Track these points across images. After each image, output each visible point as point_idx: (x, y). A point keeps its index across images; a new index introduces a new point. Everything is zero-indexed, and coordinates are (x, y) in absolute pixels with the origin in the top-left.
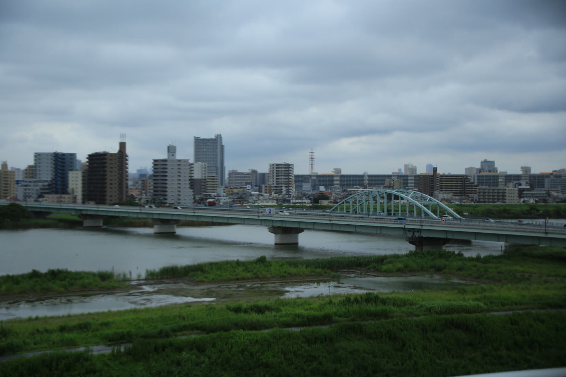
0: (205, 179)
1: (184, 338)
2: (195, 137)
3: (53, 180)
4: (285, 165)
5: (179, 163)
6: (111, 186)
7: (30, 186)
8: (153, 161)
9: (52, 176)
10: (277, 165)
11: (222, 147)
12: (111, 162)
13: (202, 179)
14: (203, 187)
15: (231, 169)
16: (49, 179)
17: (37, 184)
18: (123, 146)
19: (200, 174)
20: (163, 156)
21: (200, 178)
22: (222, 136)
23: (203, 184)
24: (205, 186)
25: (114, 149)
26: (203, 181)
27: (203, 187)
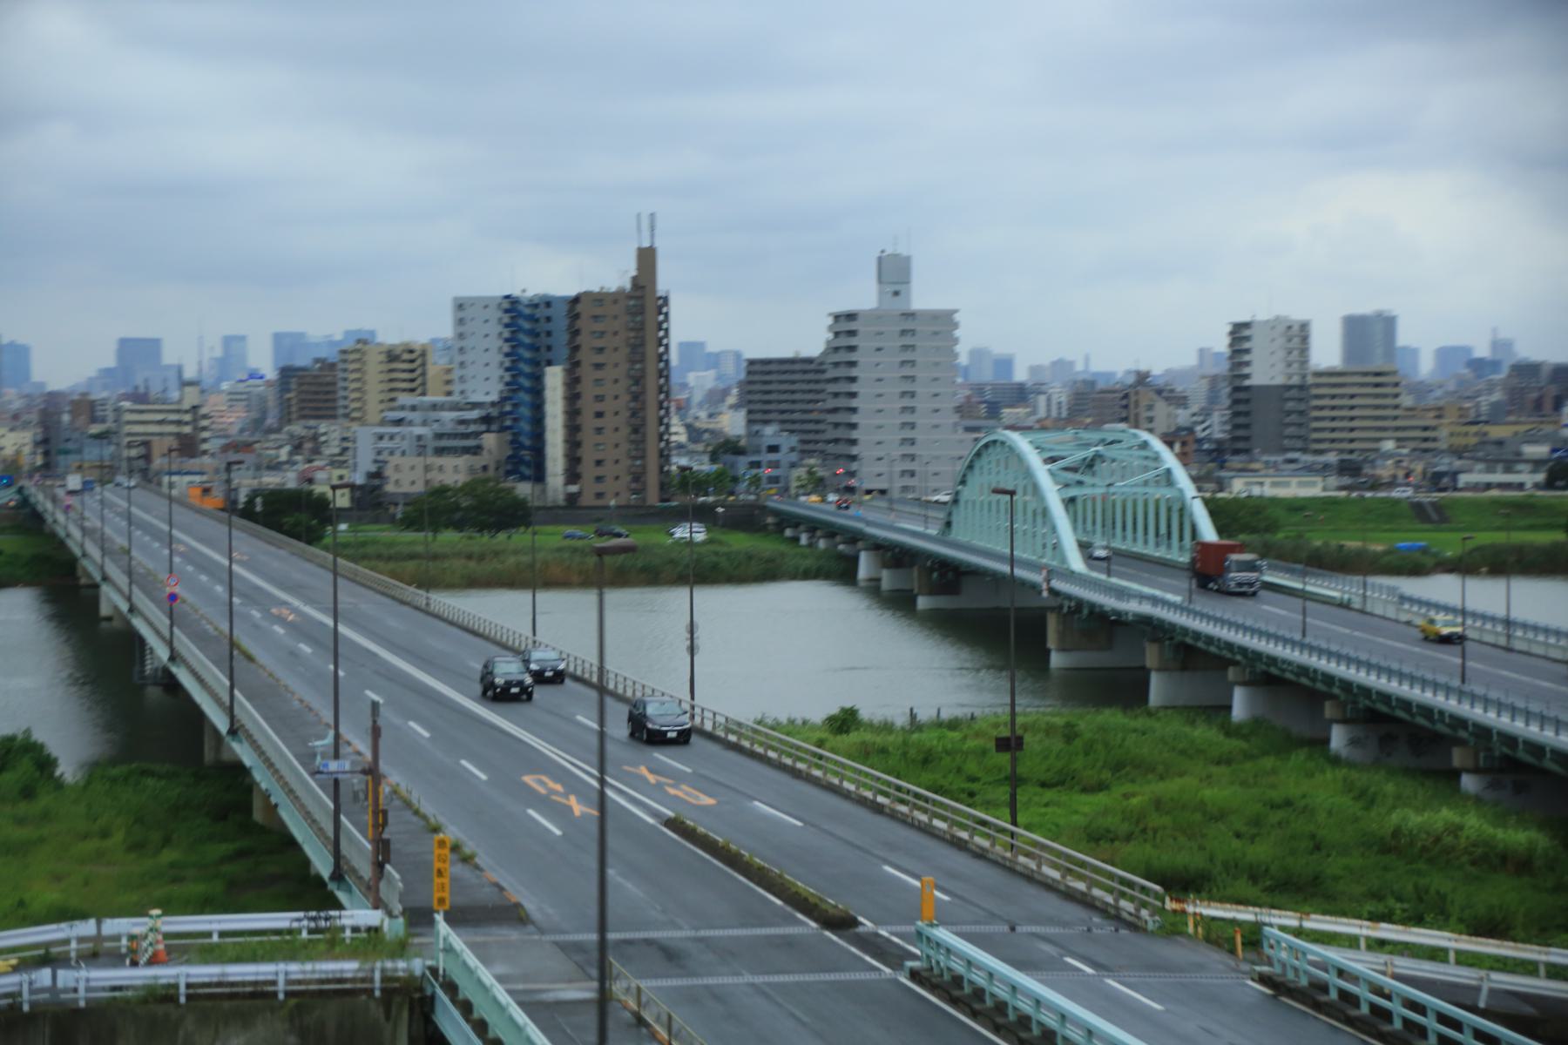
0: (1301, 387)
3: (503, 400)
5: (908, 325)
6: (599, 423)
7: (411, 423)
8: (830, 321)
9: (501, 387)
12: (599, 327)
13: (1289, 388)
14: (1294, 418)
15: (685, 339)
16: (494, 397)
18: (647, 258)
19: (1280, 366)
20: (864, 296)
21: (1279, 380)
23: (1290, 405)
24: (1301, 413)
26: (1294, 393)
27: (1294, 418)
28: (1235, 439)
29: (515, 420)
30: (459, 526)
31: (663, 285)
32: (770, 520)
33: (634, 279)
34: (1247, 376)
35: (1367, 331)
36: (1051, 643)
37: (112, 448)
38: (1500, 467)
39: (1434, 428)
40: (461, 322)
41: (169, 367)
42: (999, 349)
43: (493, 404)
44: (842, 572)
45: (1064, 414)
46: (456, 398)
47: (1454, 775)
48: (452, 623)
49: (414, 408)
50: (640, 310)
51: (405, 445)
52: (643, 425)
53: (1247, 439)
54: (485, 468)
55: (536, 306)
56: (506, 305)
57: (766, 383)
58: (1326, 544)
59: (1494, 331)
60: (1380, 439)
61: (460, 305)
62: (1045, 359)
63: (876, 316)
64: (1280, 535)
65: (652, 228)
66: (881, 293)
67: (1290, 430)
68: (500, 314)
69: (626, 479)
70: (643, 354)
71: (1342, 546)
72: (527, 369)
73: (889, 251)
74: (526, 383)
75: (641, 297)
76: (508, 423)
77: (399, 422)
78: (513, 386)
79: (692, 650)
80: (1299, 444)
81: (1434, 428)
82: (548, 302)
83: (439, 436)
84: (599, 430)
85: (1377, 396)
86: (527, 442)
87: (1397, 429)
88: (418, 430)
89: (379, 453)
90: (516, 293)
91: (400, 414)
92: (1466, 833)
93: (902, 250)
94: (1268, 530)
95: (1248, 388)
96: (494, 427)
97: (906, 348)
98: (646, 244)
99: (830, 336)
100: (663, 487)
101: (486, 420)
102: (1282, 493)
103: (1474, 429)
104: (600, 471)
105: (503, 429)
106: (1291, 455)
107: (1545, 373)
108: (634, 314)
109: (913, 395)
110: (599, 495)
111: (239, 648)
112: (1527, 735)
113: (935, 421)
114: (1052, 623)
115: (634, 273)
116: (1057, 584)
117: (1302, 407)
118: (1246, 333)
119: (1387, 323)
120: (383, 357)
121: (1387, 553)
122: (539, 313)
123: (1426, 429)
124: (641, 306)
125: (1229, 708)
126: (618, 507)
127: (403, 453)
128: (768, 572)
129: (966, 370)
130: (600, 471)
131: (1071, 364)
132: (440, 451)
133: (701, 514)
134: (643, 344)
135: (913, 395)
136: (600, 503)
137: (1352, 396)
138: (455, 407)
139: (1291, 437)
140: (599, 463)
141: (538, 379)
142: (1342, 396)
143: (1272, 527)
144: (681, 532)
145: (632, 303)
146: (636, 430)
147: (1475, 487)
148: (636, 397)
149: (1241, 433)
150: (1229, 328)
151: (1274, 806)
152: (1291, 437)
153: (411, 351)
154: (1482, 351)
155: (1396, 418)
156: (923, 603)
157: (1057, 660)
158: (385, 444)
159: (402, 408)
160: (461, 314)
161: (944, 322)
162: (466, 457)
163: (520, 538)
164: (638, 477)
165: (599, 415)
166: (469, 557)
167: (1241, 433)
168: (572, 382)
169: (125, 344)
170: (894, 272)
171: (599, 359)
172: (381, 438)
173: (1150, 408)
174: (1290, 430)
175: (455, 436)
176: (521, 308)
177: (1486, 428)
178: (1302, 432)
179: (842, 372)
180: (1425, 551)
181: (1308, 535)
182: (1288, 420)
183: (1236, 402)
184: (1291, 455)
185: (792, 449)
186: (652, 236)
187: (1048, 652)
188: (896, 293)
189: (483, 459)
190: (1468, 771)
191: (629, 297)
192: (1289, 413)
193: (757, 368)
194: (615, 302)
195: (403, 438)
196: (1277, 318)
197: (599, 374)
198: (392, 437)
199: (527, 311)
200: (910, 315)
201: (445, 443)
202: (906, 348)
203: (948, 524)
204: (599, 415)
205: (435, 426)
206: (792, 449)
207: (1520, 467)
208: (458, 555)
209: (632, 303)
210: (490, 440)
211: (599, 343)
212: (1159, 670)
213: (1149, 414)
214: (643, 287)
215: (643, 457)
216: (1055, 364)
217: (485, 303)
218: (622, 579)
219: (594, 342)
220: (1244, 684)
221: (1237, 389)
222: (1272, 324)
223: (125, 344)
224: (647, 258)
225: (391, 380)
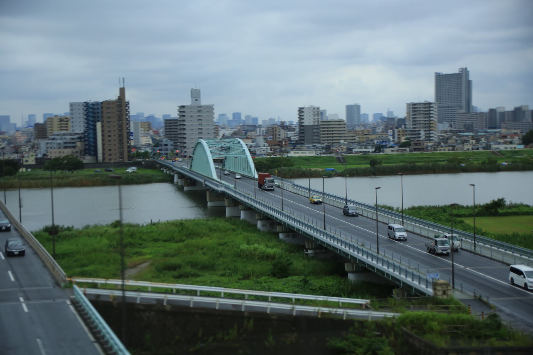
1: (442, 314)
2: (436, 73)
3: (85, 132)
4: (425, 104)
6: (110, 138)
7: (57, 139)
8: (178, 108)
9: (84, 128)
10: (414, 104)
11: (469, 83)
12: (109, 111)
13: (314, 125)
16: (82, 131)
17: (64, 137)
18: (122, 91)
19: (312, 120)
20: (188, 102)
21: (312, 124)
22: (468, 70)
23: (315, 130)
24: (318, 133)
25: (114, 96)
26: (316, 127)
27: (316, 134)
29: (89, 138)
30: (63, 169)
32: (158, 166)
33: (119, 97)
34: (303, 123)
35: (353, 110)
36: (208, 200)
37: (483, 139)
38: (363, 147)
39: (355, 136)
40: (72, 110)
41: (12, 124)
42: (254, 115)
43: (82, 133)
44: (169, 180)
45: (264, 134)
47: (277, 234)
49: (58, 135)
51: (55, 146)
52: (123, 139)
53: (303, 140)
54: (77, 152)
55: (94, 105)
56: (85, 105)
57: (170, 126)
58: (306, 169)
59: (388, 109)
60: (339, 140)
61: (71, 105)
62: (267, 118)
63: (190, 107)
64: (294, 167)
65: (124, 82)
66: (192, 100)
67: (315, 137)
68: (83, 107)
69: (118, 155)
71: (310, 170)
72: (91, 123)
73: (194, 88)
74: (91, 127)
75: (121, 102)
76: (87, 139)
77: (53, 139)
78: (88, 128)
79: (20, 207)
80: (318, 141)
81: (355, 136)
82: (97, 104)
83: (65, 143)
84: (110, 141)
85: (339, 128)
86: (92, 144)
87: (345, 137)
88: (59, 141)
89: (47, 148)
92: (259, 250)
93: (198, 88)
95: (303, 126)
96: (82, 140)
98: (122, 87)
99: (178, 112)
100: (129, 156)
101: (80, 138)
102: (297, 155)
103: (365, 136)
104: (110, 152)
105: (85, 141)
106: (314, 145)
107: (396, 120)
108: (119, 107)
109: (201, 129)
110: (110, 159)
112: (288, 223)
114: (208, 193)
115: (119, 95)
116: (207, 183)
117: (318, 131)
119: (358, 107)
120: (58, 120)
121: (322, 171)
122: (95, 107)
123: (352, 136)
124: (121, 104)
125: (240, 217)
126: (114, 163)
128: (148, 181)
129: (244, 121)
130: (110, 152)
131: (274, 119)
132: (65, 147)
133: (138, 164)
134: (122, 116)
135: (201, 129)
136: (110, 161)
137: (332, 128)
138: (71, 134)
140: (110, 150)
141: (95, 126)
142: (330, 128)
143: (292, 165)
144: (130, 170)
146: (120, 141)
147: (357, 152)
149: (302, 138)
150: (298, 109)
151: (220, 245)
153: (67, 118)
154: (385, 115)
155: (344, 134)
156: (186, 189)
157: (209, 204)
158: (49, 145)
159: (55, 135)
161: (210, 108)
162: (72, 149)
164: (122, 154)
165: (110, 136)
166: (59, 178)
167: (302, 138)
168: (103, 126)
170: (196, 94)
171: (109, 120)
172: (48, 144)
174: (315, 137)
175: (70, 143)
177: (369, 136)
178: (319, 138)
179: (182, 123)
180: (333, 171)
181: (301, 167)
183: (300, 130)
184: (314, 145)
185: (172, 145)
186: (124, 84)
187: (207, 202)
188: (196, 100)
189: (77, 149)
190: (281, 232)
193: (167, 122)
195: (54, 144)
197: (109, 124)
198: (51, 144)
199: (91, 106)
200: (200, 106)
201: (67, 145)
202: (199, 116)
203: (191, 166)
204: (110, 136)
205: (64, 140)
206: (172, 145)
207: (369, 147)
210: (79, 144)
211: (109, 115)
212: (228, 206)
215: (123, 148)
216: (269, 119)
217: (79, 104)
218: (60, 186)
219: (106, 115)
220: (244, 210)
221: (300, 126)
222: (309, 108)
224: (122, 91)
225: (61, 127)
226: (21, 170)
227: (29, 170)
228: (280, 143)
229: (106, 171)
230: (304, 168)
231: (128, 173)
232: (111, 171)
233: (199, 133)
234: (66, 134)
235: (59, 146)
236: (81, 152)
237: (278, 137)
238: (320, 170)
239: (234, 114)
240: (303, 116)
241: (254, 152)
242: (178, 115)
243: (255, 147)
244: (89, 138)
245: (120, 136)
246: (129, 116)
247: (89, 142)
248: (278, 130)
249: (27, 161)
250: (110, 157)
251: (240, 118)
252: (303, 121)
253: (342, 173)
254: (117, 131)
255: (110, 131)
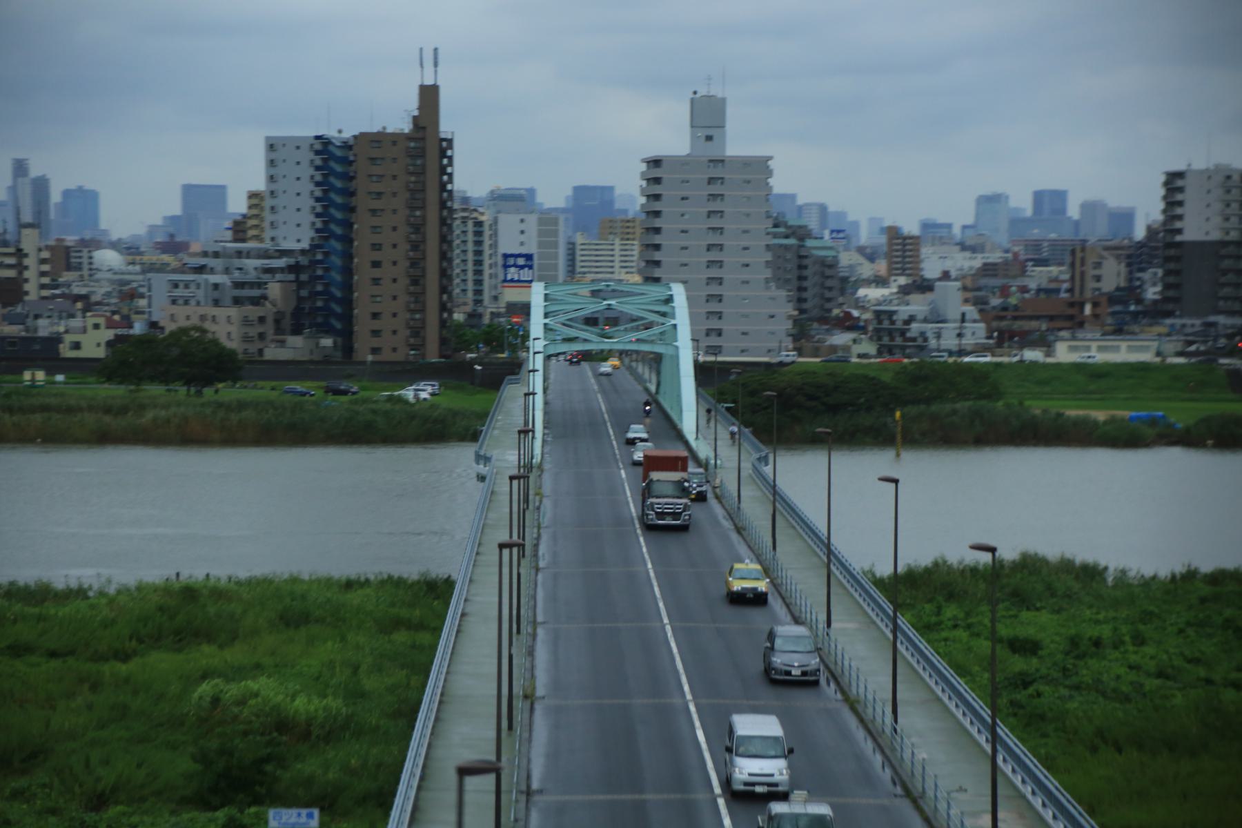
3: (314, 247)
7: (212, 271)
12: (377, 170)
13: (1223, 244)
16: (305, 245)
17: (237, 262)
18: (429, 95)
19: (1217, 220)
21: (1216, 236)
25: (397, 116)
28: (1166, 300)
29: (327, 270)
31: (446, 127)
33: (415, 119)
34: (1179, 231)
40: (271, 163)
43: (303, 252)
46: (267, 245)
48: (802, 520)
50: (421, 153)
54: (262, 320)
56: (318, 147)
58: (1045, 411)
61: (271, 146)
63: (681, 163)
64: (1000, 403)
66: (694, 138)
69: (404, 333)
70: (424, 200)
74: (338, 230)
75: (423, 139)
76: (320, 272)
77: (200, 269)
78: (324, 233)
83: (238, 285)
84: (376, 281)
86: (338, 294)
88: (213, 279)
90: (331, 133)
91: (203, 261)
93: (717, 91)
94: (988, 396)
95: (1180, 245)
97: (713, 197)
98: (429, 81)
100: (443, 342)
104: (376, 325)
111: (836, 557)
113: (745, 277)
118: (1179, 183)
126: (373, 363)
127: (198, 303)
129: (1077, 224)
135: (720, 247)
138: (265, 255)
139: (1226, 299)
140: (375, 316)
143: (994, 393)
145: (412, 144)
148: (415, 247)
150: (1163, 178)
152: (1226, 299)
158: (179, 292)
160: (273, 156)
161: (759, 167)
163: (227, 392)
164: (417, 332)
165: (376, 264)
167: (1171, 293)
169: (189, 191)
170: (708, 116)
171: (376, 204)
173: (1098, 265)
174: (1227, 291)
176: (331, 148)
180: (1153, 422)
182: (1223, 280)
189: (268, 310)
191: (408, 138)
192: (1225, 272)
194: (394, 143)
196: (1218, 168)
197: (375, 221)
199: (339, 153)
200: (719, 162)
202: (713, 197)
208: (91, 408)
209: (412, 144)
213: (1097, 272)
214: (424, 128)
215: (422, 311)
217: (296, 144)
222: (1208, 174)
223: (189, 191)
224: (429, 95)
226: (27, 376)
227: (60, 378)
228: (1070, 311)
229: (328, 390)
230: (1036, 407)
231: (402, 400)
232: (345, 393)
233: (710, 264)
234: (248, 254)
235: (216, 294)
236: (277, 322)
237: (1091, 284)
238: (1100, 416)
239: (1039, 197)
240: (1180, 204)
241: (920, 342)
242: (643, 192)
243: (925, 321)
244: (327, 270)
245: (414, 264)
246: (451, 192)
247: (327, 285)
248: (1091, 260)
249: (77, 346)
250: (375, 342)
251: (1063, 211)
252: (1178, 225)
253: (1188, 430)
254: (404, 246)
255: (376, 247)
